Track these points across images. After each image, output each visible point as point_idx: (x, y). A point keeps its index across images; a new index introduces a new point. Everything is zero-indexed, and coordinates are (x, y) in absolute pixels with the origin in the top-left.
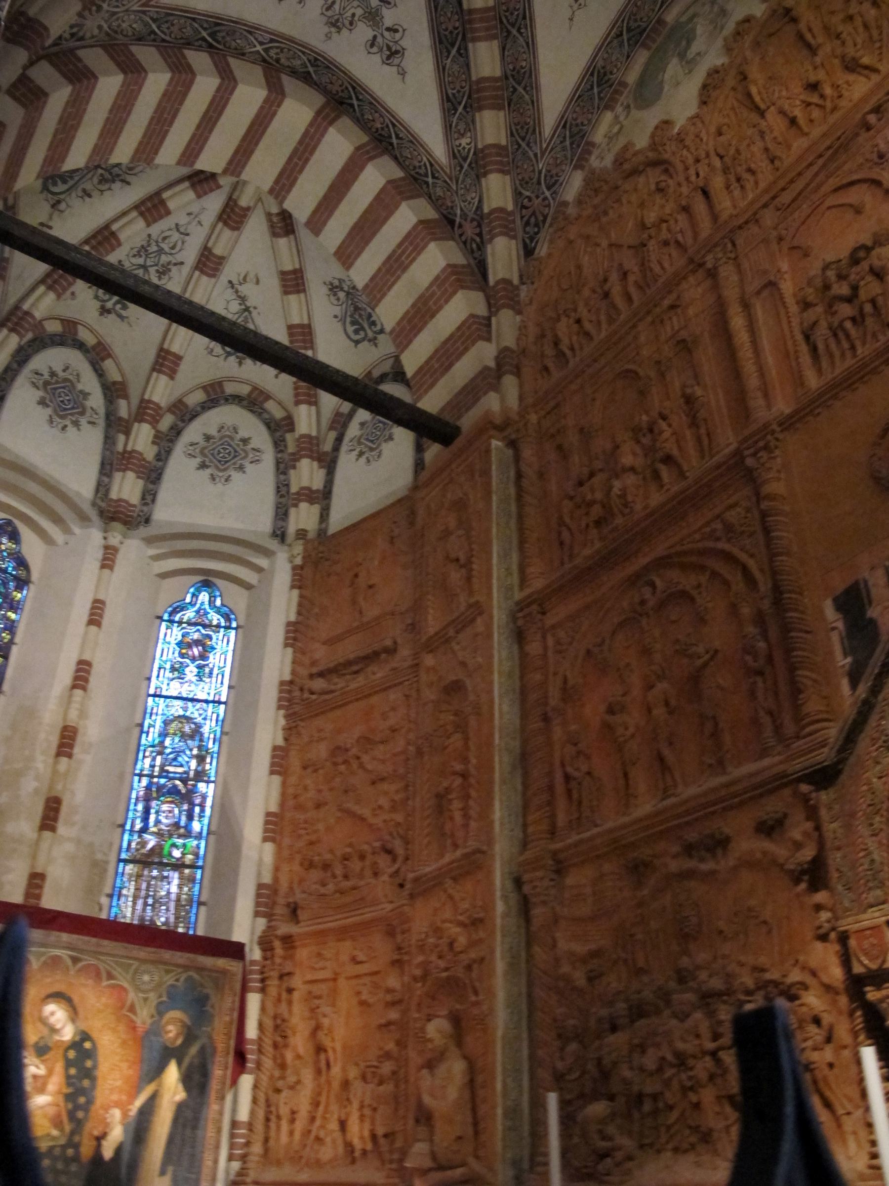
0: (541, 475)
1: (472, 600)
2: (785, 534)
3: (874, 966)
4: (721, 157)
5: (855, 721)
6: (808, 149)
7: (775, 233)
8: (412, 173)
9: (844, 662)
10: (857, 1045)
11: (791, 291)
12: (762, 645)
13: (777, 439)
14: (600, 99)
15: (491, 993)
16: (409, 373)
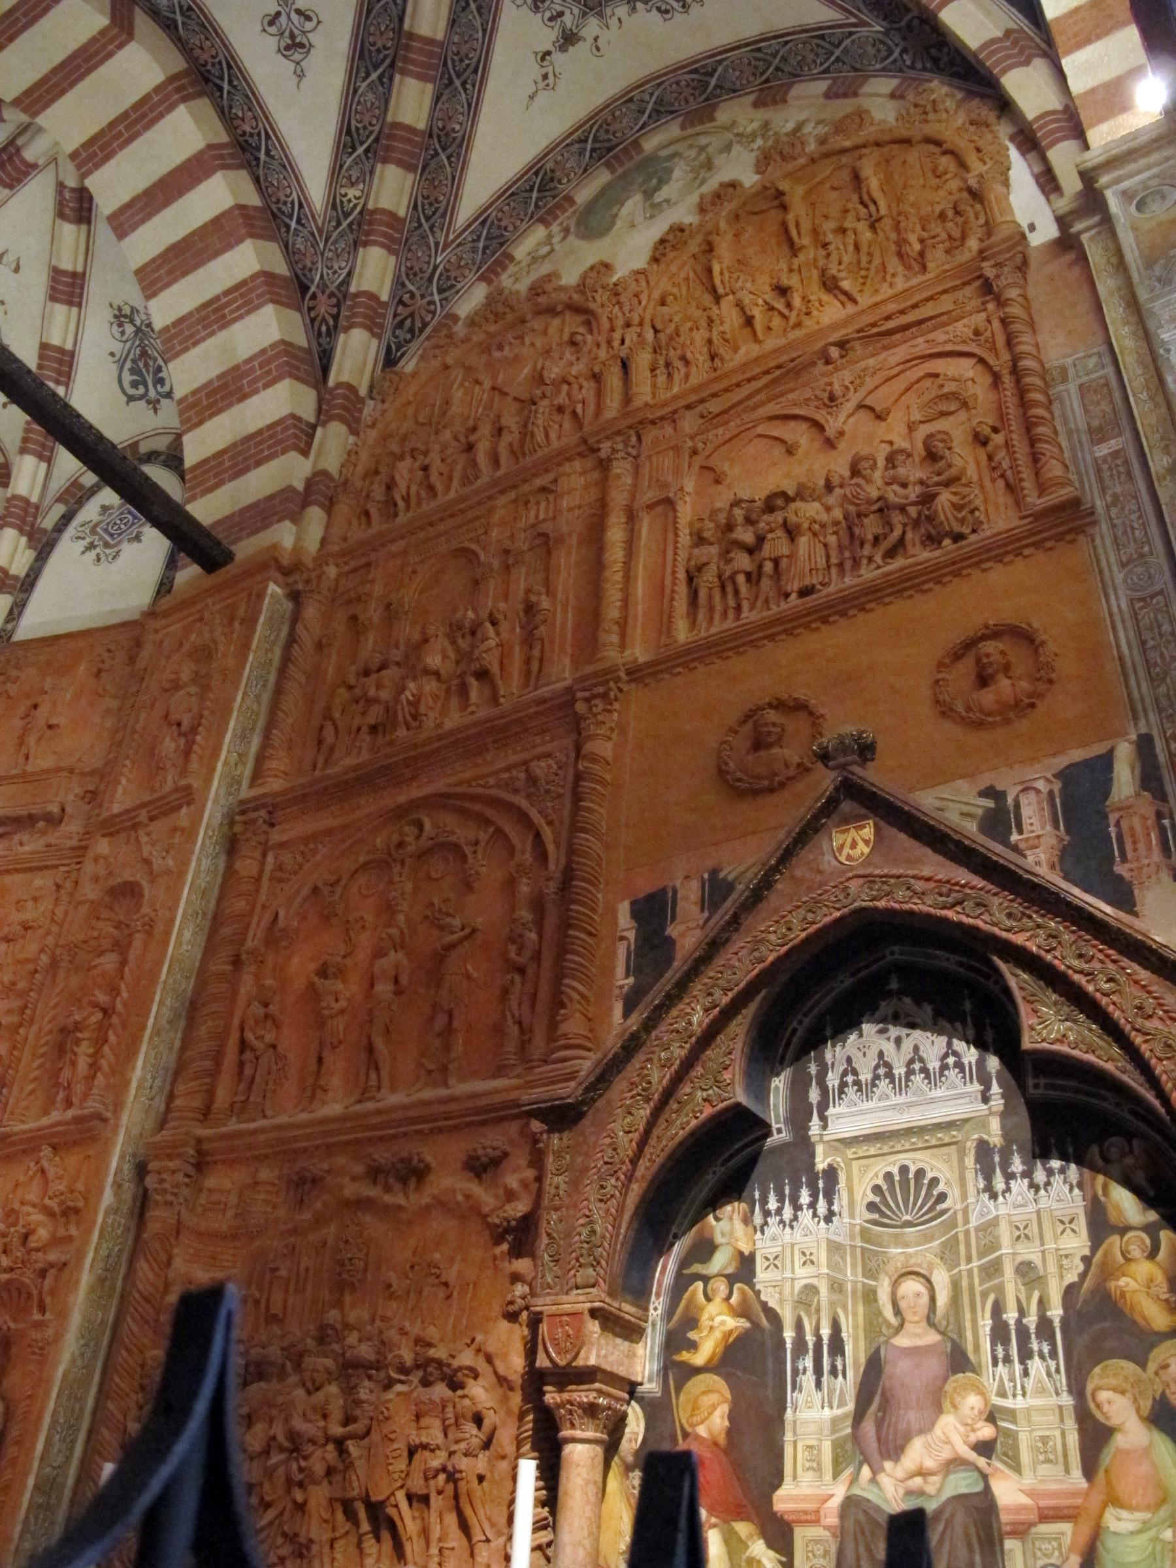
0: (320, 646)
1: (183, 782)
3: (562, 1362)
4: (656, 331)
5: (616, 1055)
6: (756, 360)
7: (690, 444)
8: (274, 207)
9: (624, 981)
11: (689, 518)
12: (533, 936)
13: (620, 690)
14: (536, 205)
15: (63, 1315)
16: (188, 462)
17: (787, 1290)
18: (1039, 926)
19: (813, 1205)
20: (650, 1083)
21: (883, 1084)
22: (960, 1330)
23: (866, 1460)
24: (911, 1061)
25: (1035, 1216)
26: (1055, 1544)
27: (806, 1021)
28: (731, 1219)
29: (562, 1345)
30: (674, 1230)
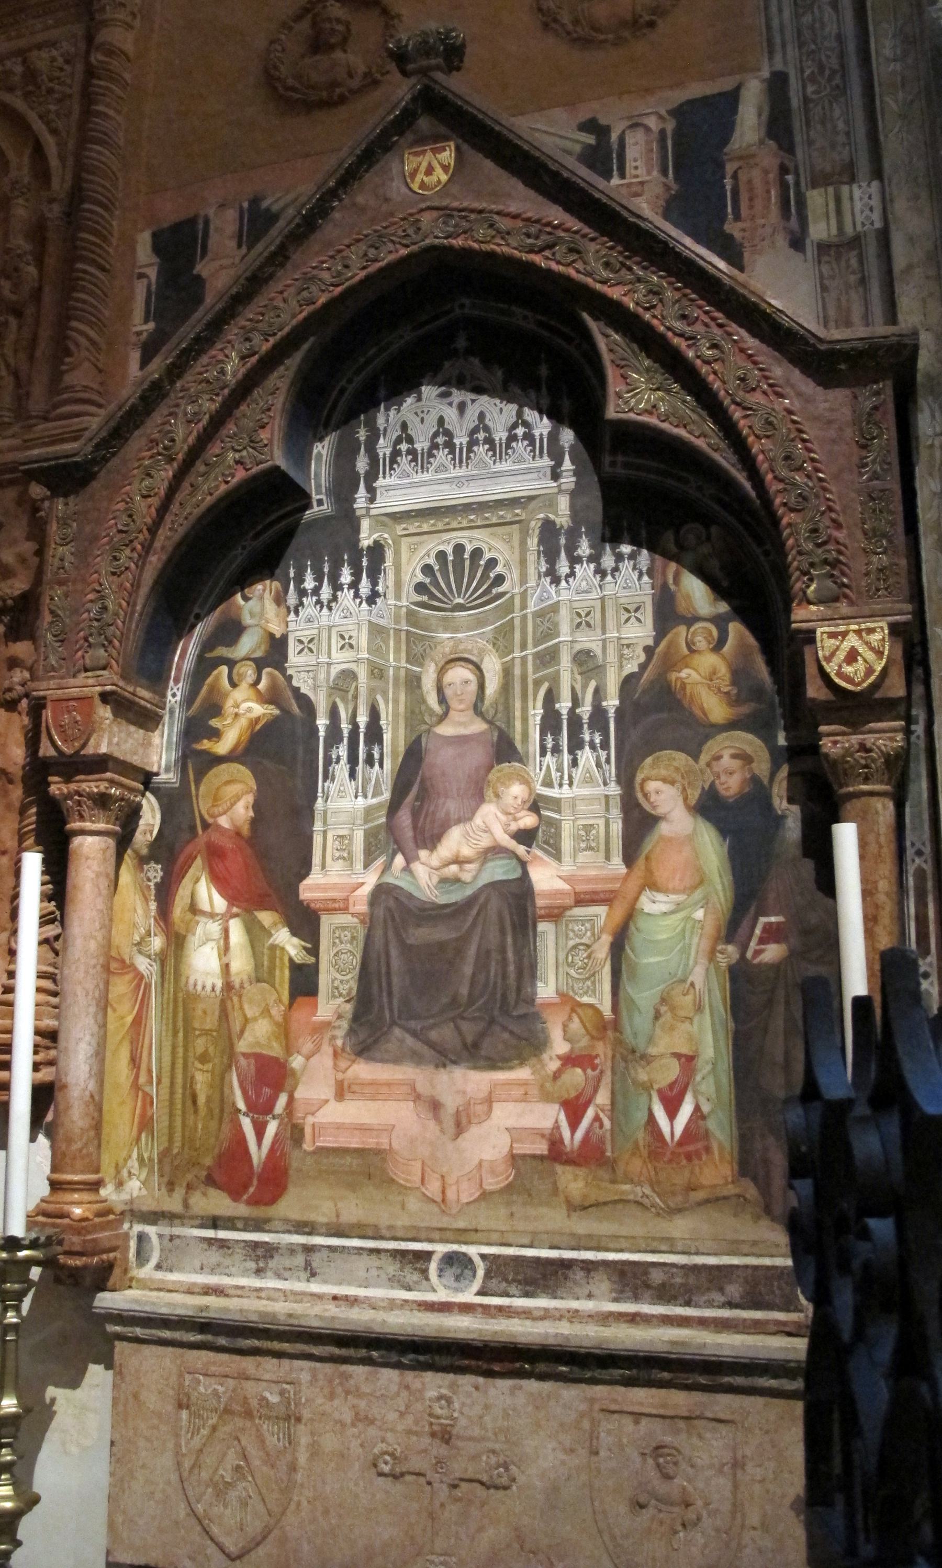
2: (111, 113)
3: (67, 750)
5: (133, 408)
9: (143, 327)
10: (21, 850)
12: (32, 270)
17: (322, 676)
18: (639, 280)
19: (354, 585)
20: (173, 440)
21: (442, 455)
22: (509, 720)
23: (400, 849)
24: (475, 430)
25: (598, 604)
26: (588, 925)
27: (358, 379)
28: (261, 598)
29: (70, 732)
30: (196, 610)
